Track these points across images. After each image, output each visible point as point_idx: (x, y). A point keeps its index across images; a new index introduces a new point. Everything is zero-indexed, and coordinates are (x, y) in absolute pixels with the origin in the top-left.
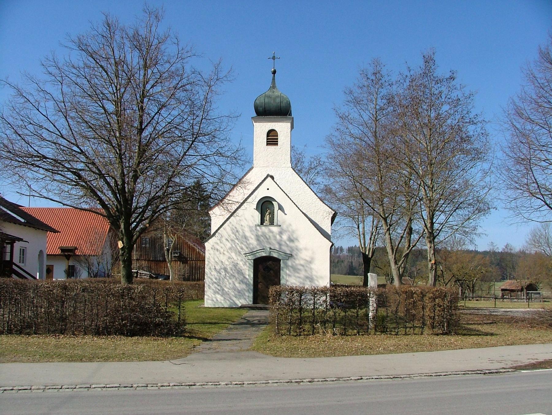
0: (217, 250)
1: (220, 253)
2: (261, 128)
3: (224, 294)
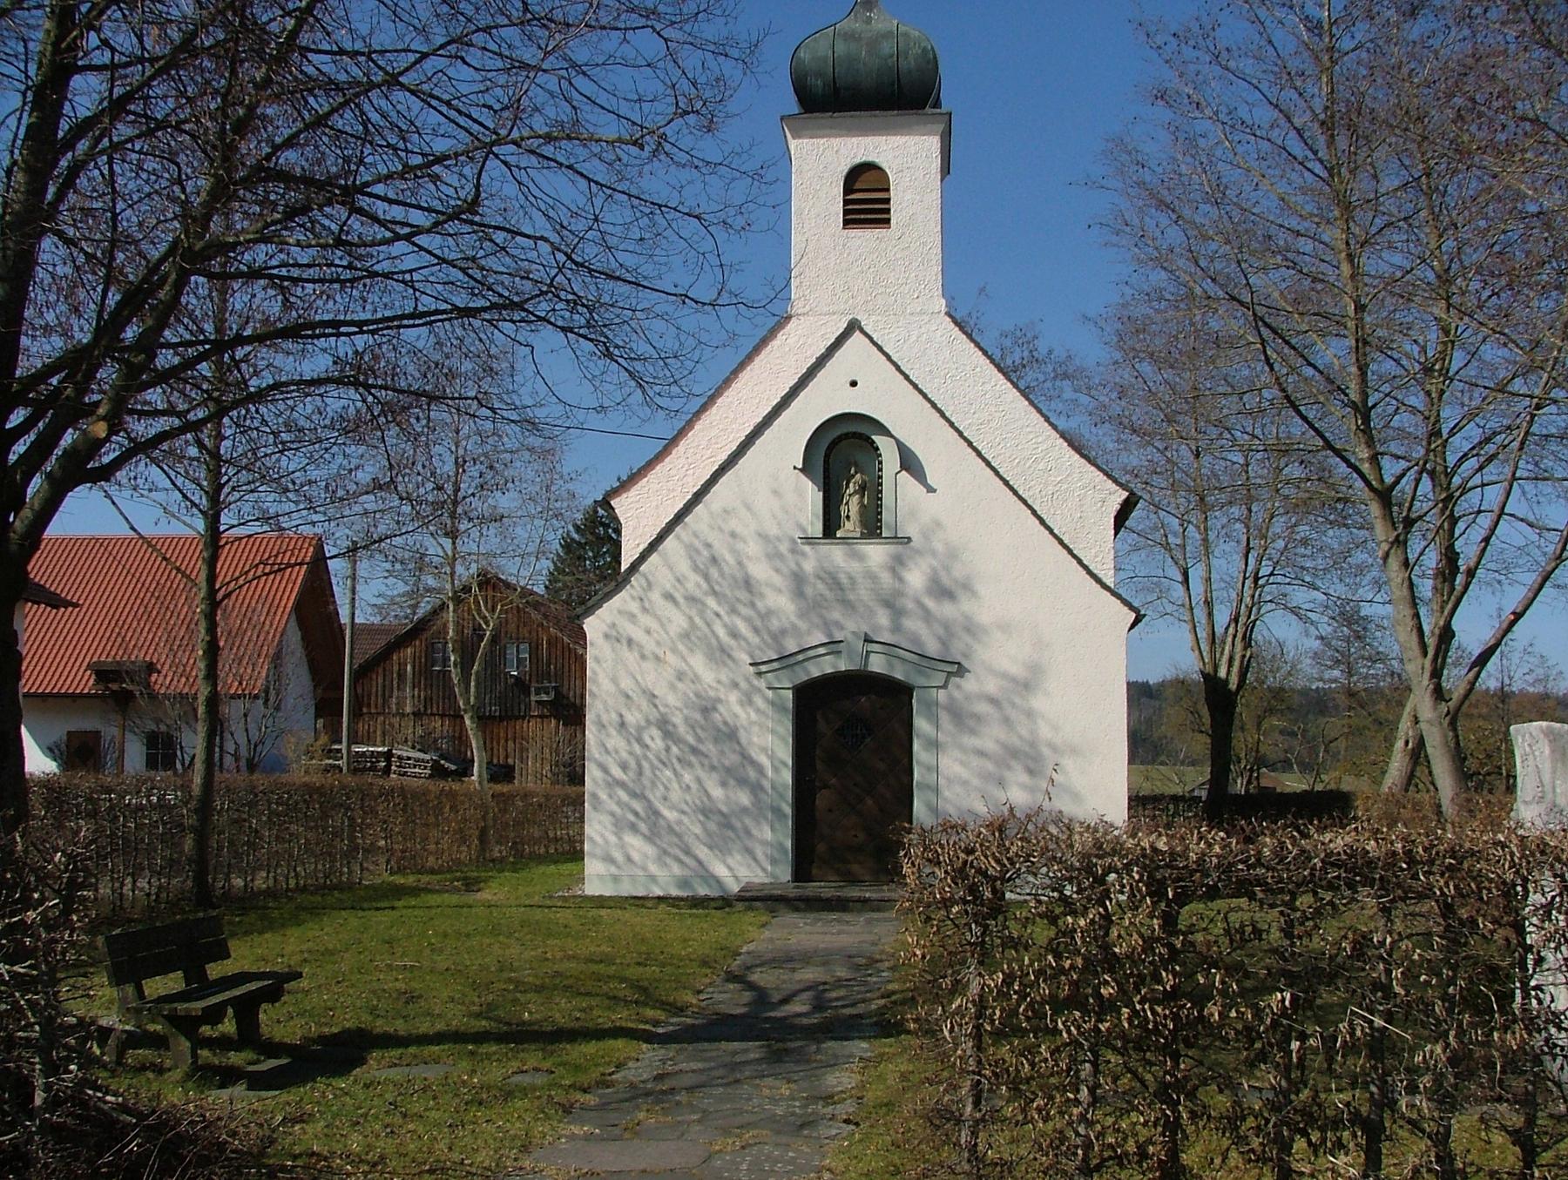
0: (630, 642)
1: (643, 657)
2: (820, 161)
3: (653, 826)
